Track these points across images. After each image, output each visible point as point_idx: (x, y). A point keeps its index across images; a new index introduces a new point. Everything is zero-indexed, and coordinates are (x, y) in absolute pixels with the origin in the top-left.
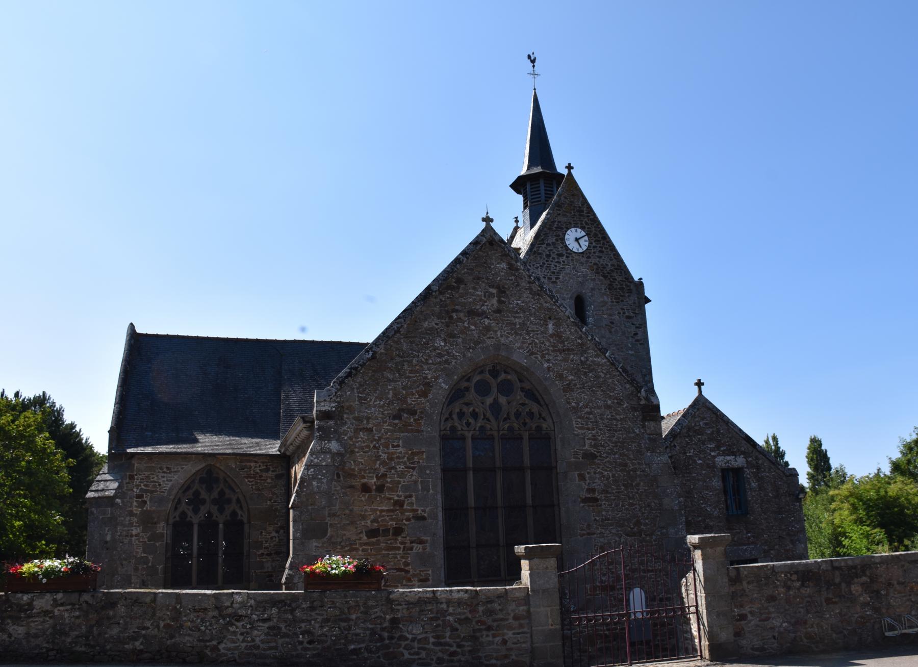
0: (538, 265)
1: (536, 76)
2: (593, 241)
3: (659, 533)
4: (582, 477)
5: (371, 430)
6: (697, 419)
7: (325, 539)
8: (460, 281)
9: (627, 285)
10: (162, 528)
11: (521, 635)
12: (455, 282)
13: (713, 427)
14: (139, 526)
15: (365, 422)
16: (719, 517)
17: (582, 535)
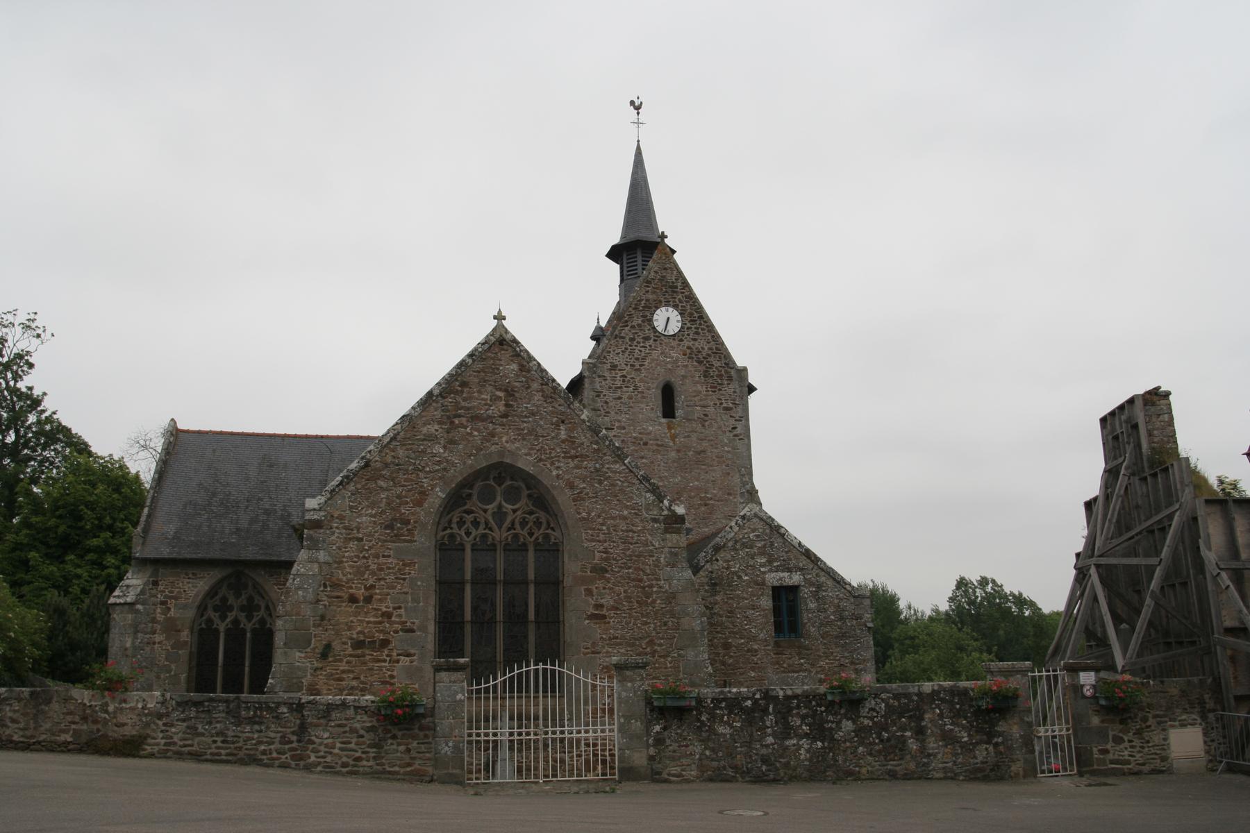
0: (620, 351)
1: (640, 125)
2: (687, 322)
3: (676, 655)
4: (589, 592)
5: (361, 540)
6: (746, 531)
7: (309, 650)
8: (464, 384)
9: (726, 372)
10: (185, 635)
11: (426, 745)
12: (459, 386)
13: (765, 540)
14: (162, 634)
16: (766, 641)
17: (585, 654)
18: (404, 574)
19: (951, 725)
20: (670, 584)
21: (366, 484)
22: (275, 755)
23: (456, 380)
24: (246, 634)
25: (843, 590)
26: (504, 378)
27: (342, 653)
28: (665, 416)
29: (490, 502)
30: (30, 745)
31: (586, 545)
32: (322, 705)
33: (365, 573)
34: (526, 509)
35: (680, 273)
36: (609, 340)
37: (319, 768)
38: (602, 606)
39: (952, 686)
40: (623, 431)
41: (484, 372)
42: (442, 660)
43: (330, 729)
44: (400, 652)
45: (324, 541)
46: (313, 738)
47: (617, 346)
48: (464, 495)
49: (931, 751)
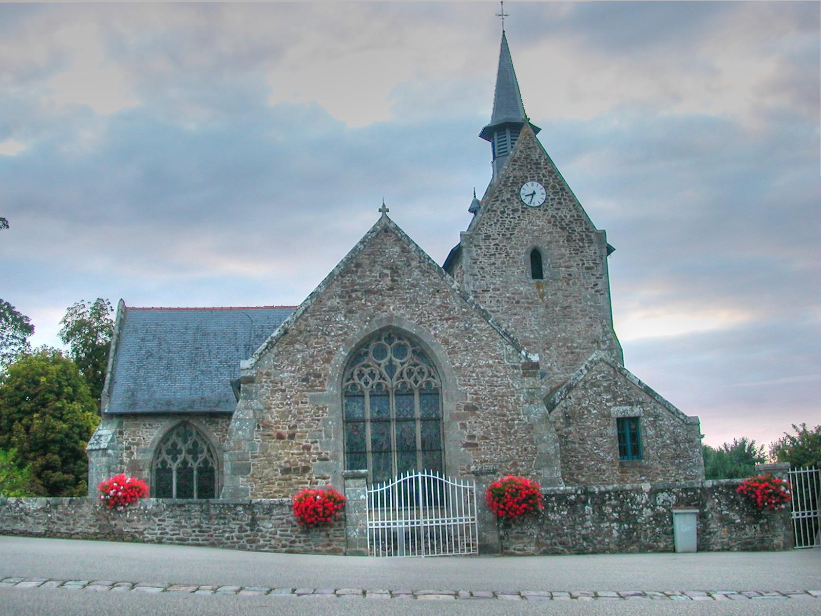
2: (551, 194)
3: (535, 474)
4: (463, 426)
5: (284, 391)
6: (594, 373)
7: (249, 475)
8: (358, 265)
9: (587, 236)
12: (354, 267)
15: (280, 385)
16: (612, 462)
18: (319, 416)
19: (727, 510)
20: (528, 418)
21: (286, 348)
22: (235, 540)
23: (352, 262)
24: (193, 471)
25: (677, 419)
26: (389, 259)
27: (274, 478)
28: (534, 276)
29: (382, 358)
30: (71, 535)
31: (460, 389)
32: (265, 504)
33: (288, 417)
34: (411, 361)
35: (543, 151)
36: (483, 214)
37: (266, 549)
38: (473, 437)
39: (727, 482)
40: (498, 292)
41: (373, 254)
42: (349, 471)
43: (273, 521)
44: (318, 476)
45: (256, 393)
46: (261, 528)
47: (489, 219)
48: (362, 353)
49: (712, 530)
